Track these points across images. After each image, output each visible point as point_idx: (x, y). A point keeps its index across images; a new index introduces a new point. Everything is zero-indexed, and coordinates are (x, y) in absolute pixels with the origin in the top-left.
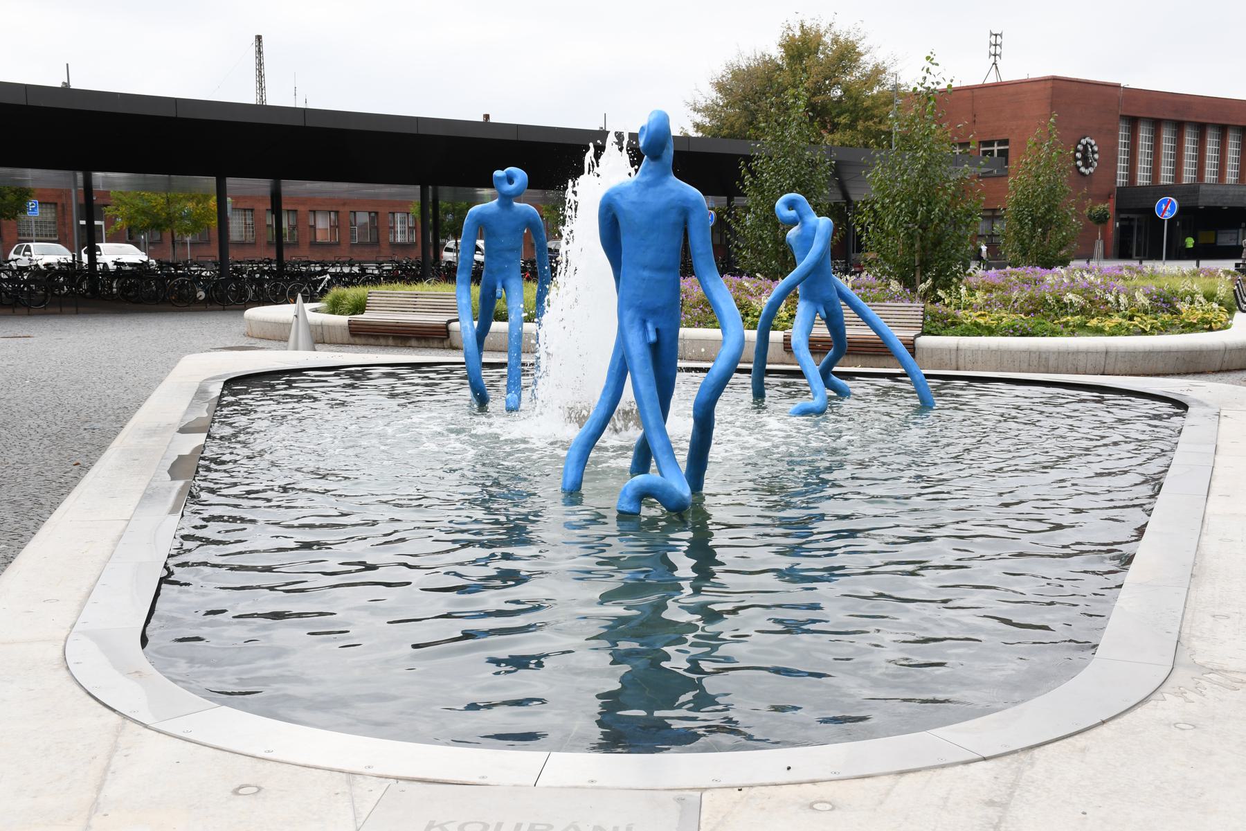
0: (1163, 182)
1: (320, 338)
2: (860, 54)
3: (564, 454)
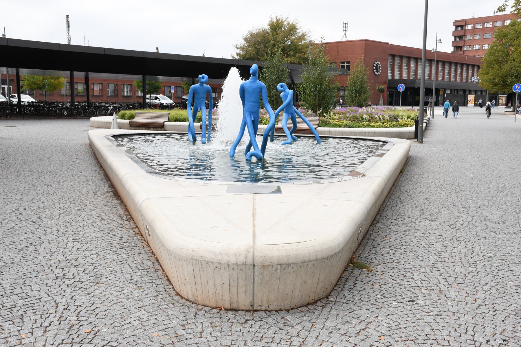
0: (404, 78)
1: (120, 127)
2: (297, 29)
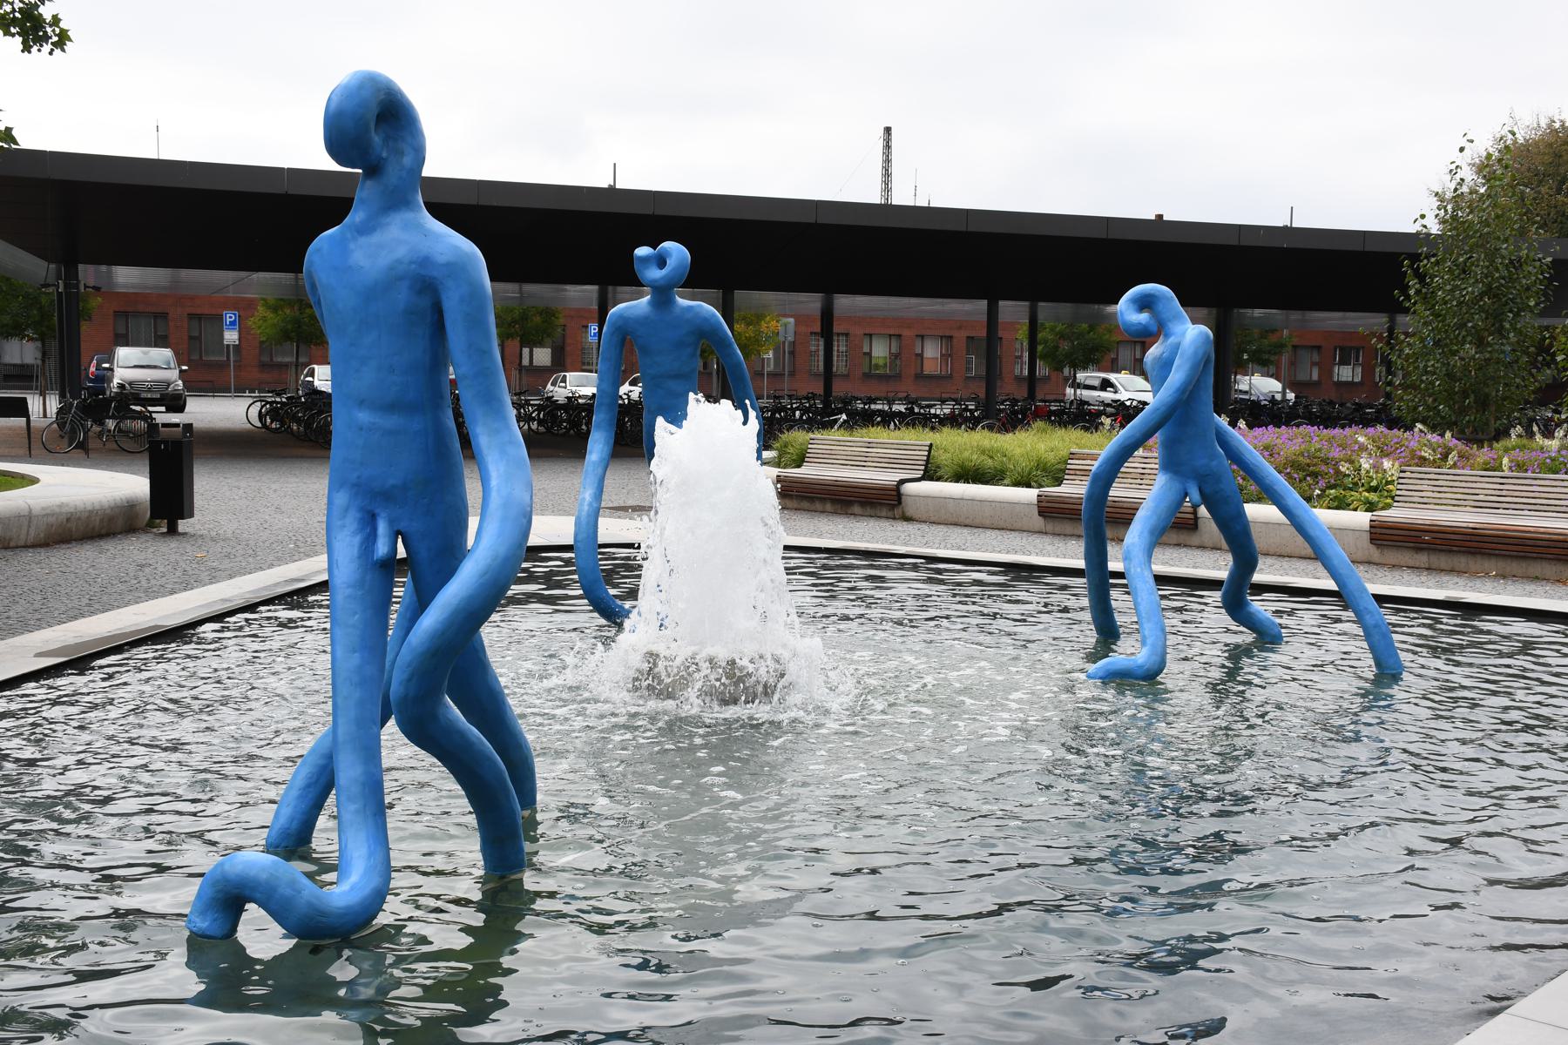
3: (285, 774)
